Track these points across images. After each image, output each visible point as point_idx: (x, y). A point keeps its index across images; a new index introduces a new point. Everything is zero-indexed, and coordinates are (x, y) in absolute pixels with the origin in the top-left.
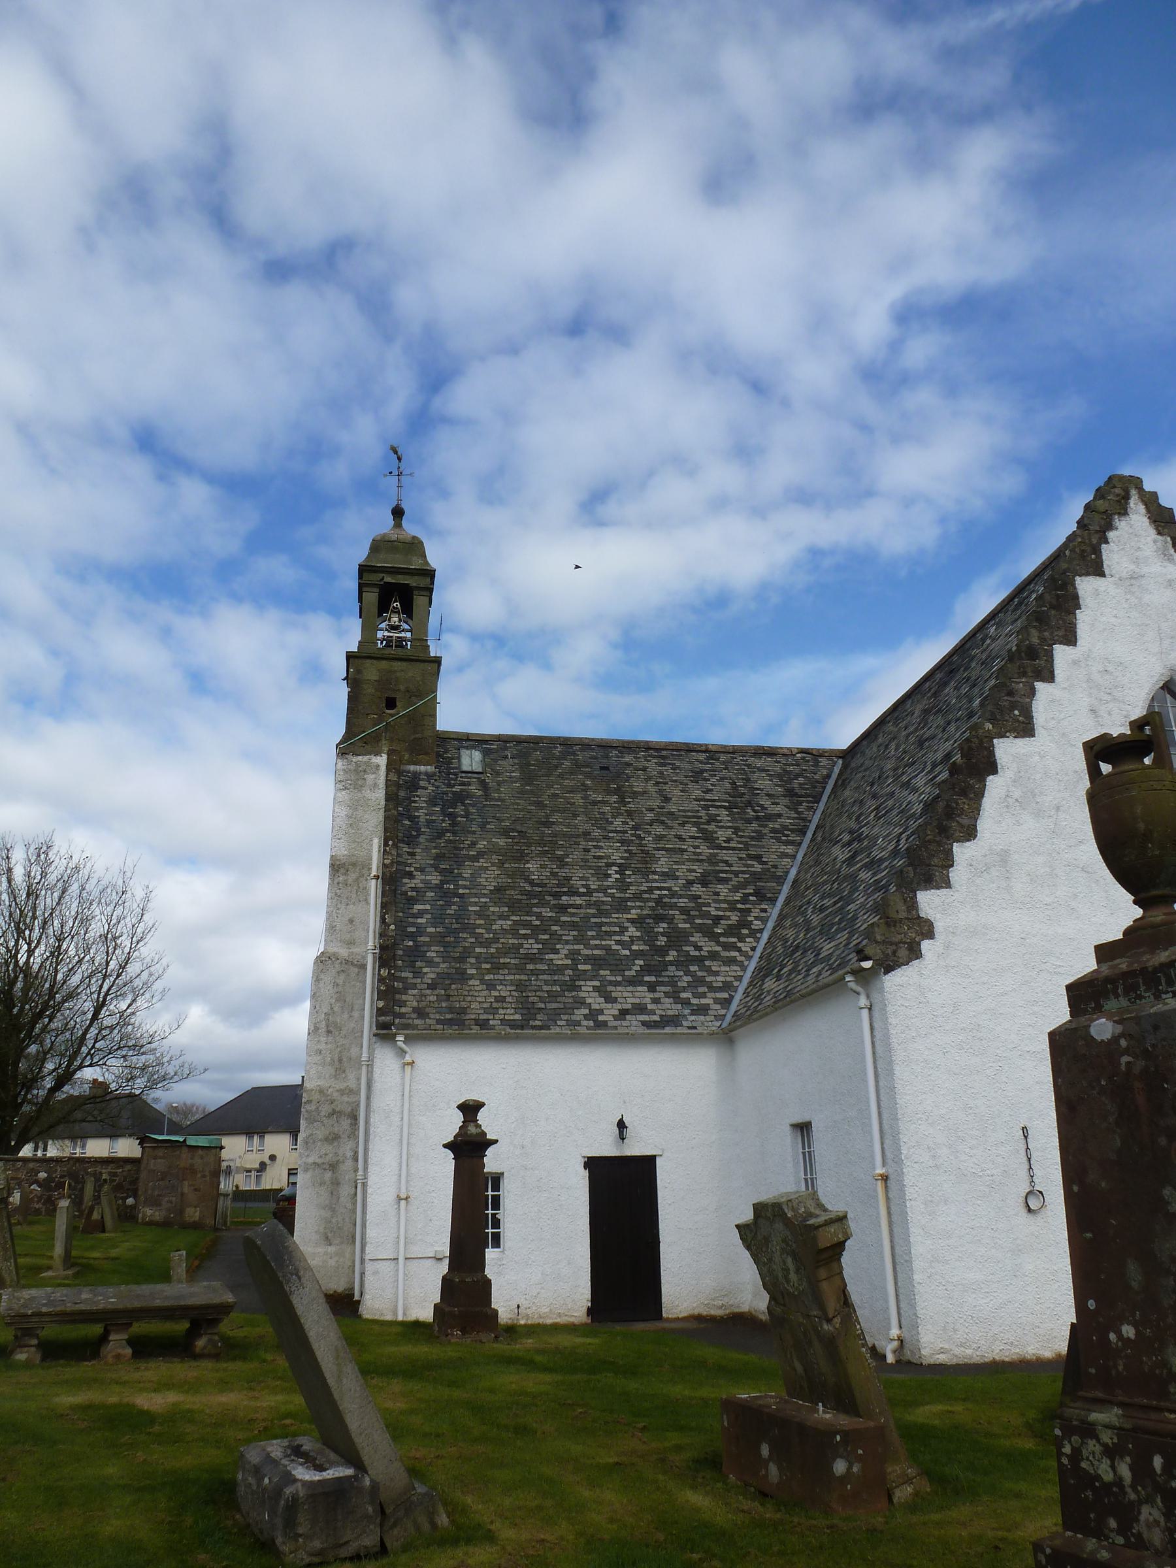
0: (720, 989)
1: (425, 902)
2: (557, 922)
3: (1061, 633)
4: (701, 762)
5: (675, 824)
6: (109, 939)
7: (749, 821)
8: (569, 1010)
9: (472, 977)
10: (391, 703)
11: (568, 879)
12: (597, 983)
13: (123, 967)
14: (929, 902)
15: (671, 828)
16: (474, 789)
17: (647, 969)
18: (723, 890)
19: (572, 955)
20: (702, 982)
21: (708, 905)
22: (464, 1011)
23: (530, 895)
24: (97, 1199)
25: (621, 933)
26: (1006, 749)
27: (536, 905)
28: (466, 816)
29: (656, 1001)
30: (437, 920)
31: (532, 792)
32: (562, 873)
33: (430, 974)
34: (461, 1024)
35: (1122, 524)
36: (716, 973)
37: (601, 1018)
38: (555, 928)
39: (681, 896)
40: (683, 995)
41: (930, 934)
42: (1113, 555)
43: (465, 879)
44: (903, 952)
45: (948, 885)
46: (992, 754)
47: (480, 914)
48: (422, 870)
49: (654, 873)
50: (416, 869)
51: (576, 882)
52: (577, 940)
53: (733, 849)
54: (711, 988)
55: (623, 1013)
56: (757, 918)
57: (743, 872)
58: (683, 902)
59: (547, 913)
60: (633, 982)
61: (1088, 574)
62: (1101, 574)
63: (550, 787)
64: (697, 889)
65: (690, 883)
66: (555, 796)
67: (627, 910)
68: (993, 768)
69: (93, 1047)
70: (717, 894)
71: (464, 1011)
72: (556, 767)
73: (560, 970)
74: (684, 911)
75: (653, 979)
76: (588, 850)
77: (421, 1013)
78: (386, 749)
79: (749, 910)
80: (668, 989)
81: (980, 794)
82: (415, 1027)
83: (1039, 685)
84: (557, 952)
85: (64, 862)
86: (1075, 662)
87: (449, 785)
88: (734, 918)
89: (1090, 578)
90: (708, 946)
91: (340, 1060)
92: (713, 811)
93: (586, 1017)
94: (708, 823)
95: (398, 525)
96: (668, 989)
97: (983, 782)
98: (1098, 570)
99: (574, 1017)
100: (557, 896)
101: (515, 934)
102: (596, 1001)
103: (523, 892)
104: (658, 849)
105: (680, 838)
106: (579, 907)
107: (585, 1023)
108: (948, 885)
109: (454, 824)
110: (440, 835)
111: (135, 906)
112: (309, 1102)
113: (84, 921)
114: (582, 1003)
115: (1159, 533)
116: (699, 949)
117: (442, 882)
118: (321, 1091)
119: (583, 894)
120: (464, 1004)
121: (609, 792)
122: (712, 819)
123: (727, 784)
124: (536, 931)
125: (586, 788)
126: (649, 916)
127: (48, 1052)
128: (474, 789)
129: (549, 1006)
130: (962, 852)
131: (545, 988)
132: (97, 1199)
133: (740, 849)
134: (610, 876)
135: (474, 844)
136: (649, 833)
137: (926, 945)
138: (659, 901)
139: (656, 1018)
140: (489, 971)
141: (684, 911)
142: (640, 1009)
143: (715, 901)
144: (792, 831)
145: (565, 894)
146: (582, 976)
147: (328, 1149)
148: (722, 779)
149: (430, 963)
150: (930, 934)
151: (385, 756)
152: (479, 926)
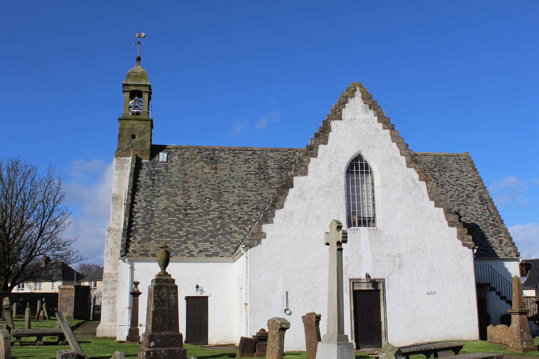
0: (235, 243)
1: (140, 213)
2: (183, 219)
3: (322, 141)
4: (249, 155)
5: (233, 181)
6: (45, 202)
7: (261, 180)
8: (182, 250)
9: (152, 239)
10: (134, 137)
11: (190, 204)
12: (193, 241)
13: (51, 213)
14: (265, 228)
15: (232, 183)
16: (163, 169)
17: (211, 236)
18: (245, 207)
19: (188, 232)
20: (230, 241)
21: (238, 213)
22: (148, 251)
23: (176, 210)
24: (41, 309)
25: (205, 224)
26: (297, 180)
27: (177, 214)
28: (158, 180)
29: (212, 247)
30: (144, 219)
31: (183, 170)
32: (189, 202)
33: (139, 238)
34: (147, 255)
35: (351, 101)
36: (235, 238)
37: (192, 253)
38: (182, 222)
39: (229, 210)
40: (222, 245)
41: (265, 237)
42: (347, 113)
43: (154, 204)
44: (256, 242)
45: (272, 223)
46: (292, 182)
47: (158, 217)
48: (140, 201)
49: (221, 201)
50: (138, 201)
51: (193, 205)
52: (189, 226)
53: (252, 191)
54: (232, 243)
55: (200, 251)
56: (254, 218)
57: (254, 200)
58: (229, 212)
59: (181, 216)
60: (206, 241)
61: (335, 119)
62: (341, 119)
63: (190, 167)
64: (236, 207)
65: (234, 204)
66: (192, 171)
67: (209, 215)
68: (292, 186)
69: (40, 247)
70: (242, 209)
71: (148, 251)
72: (194, 159)
73: (182, 237)
74: (229, 216)
75: (213, 240)
76: (199, 193)
77: (134, 252)
78: (132, 154)
79: (252, 215)
80: (217, 243)
81: (286, 195)
82: (132, 257)
83: (312, 159)
84: (182, 230)
85: (24, 169)
86: (326, 150)
87: (154, 168)
88: (246, 217)
89: (336, 121)
90: (235, 228)
91: (116, 264)
92: (249, 176)
93: (188, 253)
94: (246, 181)
95: (5, 309)
96: (217, 243)
97: (288, 190)
98: (340, 118)
99: (184, 253)
100: (185, 210)
101: (169, 224)
102: (192, 247)
103: (174, 208)
104: (225, 192)
105: (234, 187)
106: (192, 214)
107: (187, 255)
108: (272, 223)
109: (153, 183)
110: (149, 187)
111: (55, 187)
112: (105, 277)
113: (33, 194)
114: (187, 248)
115: (365, 103)
116: (231, 229)
117: (147, 206)
118: (109, 274)
119: (195, 209)
120: (148, 249)
121: (212, 169)
122: (248, 179)
123: (257, 164)
124: (176, 223)
125: (204, 167)
126: (216, 217)
127: (22, 248)
128: (163, 169)
129: (176, 249)
130: (278, 213)
131: (176, 243)
132: (41, 309)
133: (255, 191)
134: (205, 202)
135: (159, 191)
136: (223, 185)
137: (263, 240)
138: (221, 211)
139: (211, 253)
140: (158, 237)
141: (229, 216)
142: (206, 250)
143: (241, 212)
144: (276, 183)
145: (188, 209)
146: (189, 239)
147: (111, 292)
148: (256, 162)
149: (140, 235)
150: (265, 237)
151: (131, 157)
152: (157, 222)
